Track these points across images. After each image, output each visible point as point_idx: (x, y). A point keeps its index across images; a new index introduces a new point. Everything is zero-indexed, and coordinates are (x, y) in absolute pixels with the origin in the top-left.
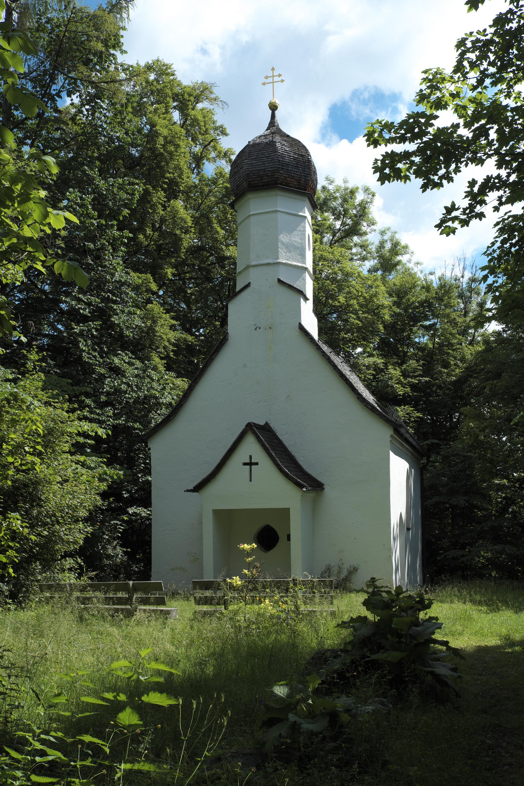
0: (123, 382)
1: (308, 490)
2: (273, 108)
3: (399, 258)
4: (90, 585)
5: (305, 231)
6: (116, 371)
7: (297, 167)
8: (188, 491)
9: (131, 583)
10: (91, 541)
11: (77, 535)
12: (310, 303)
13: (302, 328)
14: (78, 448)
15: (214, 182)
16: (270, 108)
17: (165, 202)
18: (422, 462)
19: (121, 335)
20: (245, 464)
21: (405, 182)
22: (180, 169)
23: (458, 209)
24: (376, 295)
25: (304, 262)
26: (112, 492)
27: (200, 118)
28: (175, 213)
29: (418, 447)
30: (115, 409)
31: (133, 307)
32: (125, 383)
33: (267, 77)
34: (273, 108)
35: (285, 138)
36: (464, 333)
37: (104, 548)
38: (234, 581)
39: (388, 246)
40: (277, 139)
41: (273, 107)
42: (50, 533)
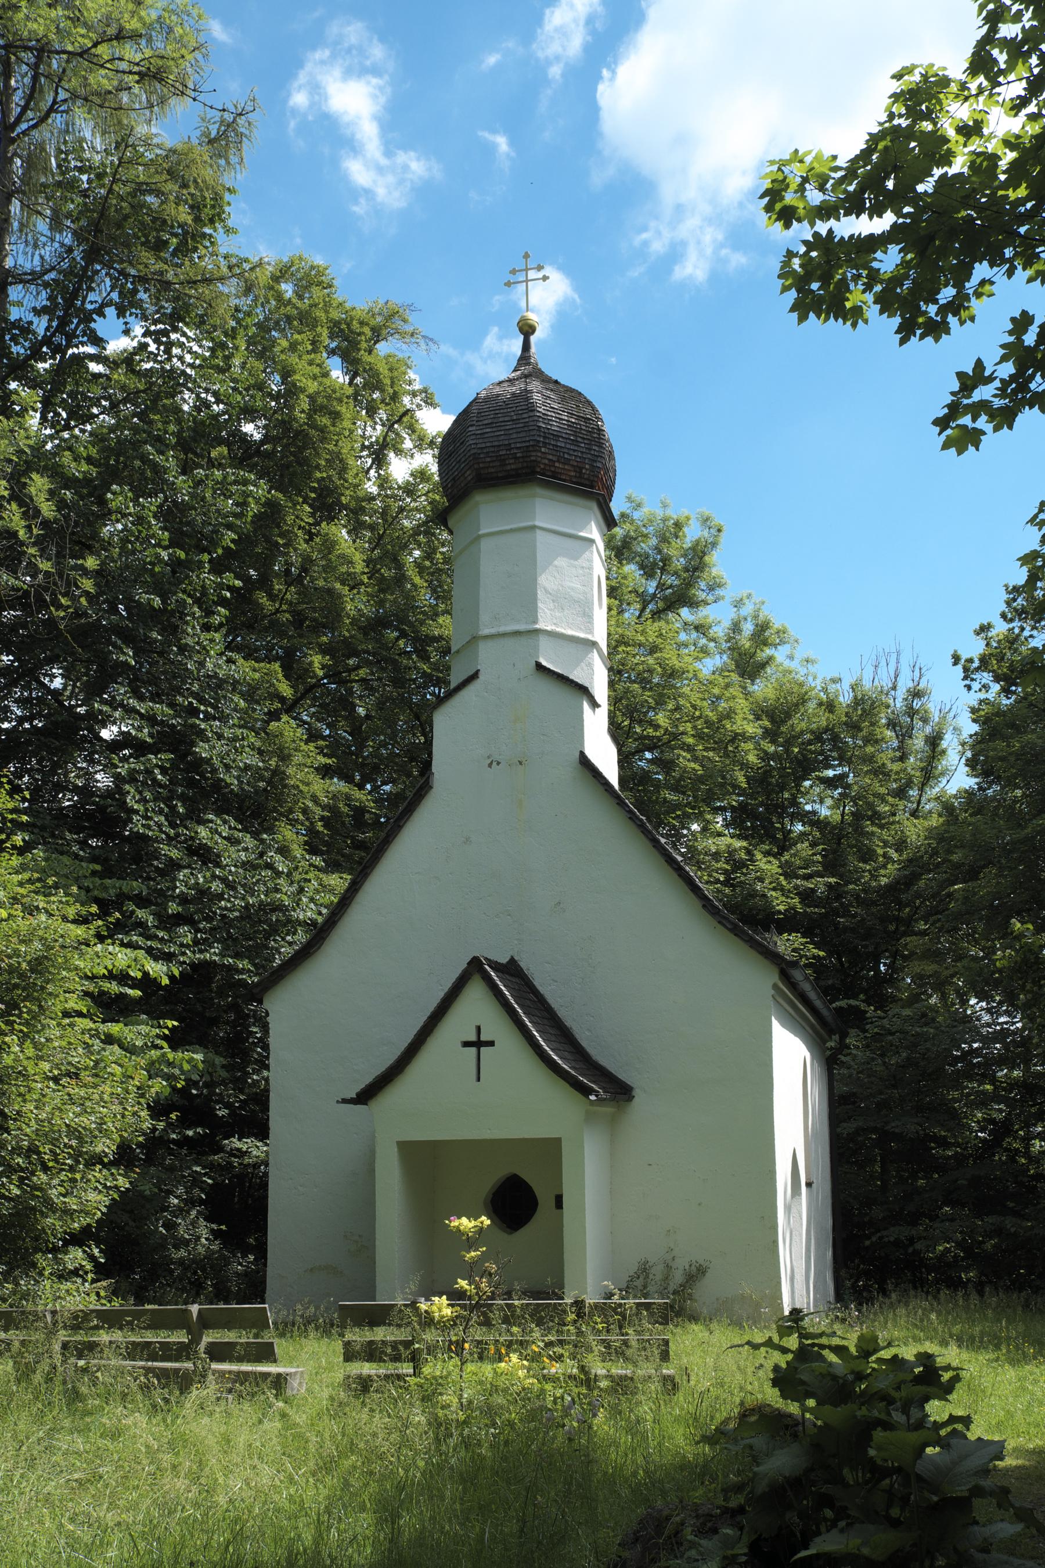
0: (214, 877)
1: (600, 1100)
3: (769, 651)
4: (100, 1314)
5: (591, 568)
6: (205, 855)
7: (575, 442)
8: (344, 1101)
9: (195, 1309)
10: (125, 1205)
11: (93, 1197)
12: (603, 712)
13: (585, 763)
14: (111, 1007)
15: (409, 490)
16: (521, 330)
17: (310, 524)
18: (829, 1044)
19: (218, 785)
20: (467, 1044)
21: (854, 325)
22: (341, 461)
23: (990, 379)
24: (729, 715)
25: (591, 632)
26: (183, 1105)
27: (383, 369)
28: (329, 545)
29: (825, 1012)
30: (198, 930)
31: (240, 727)
32: (219, 877)
33: (513, 272)
35: (551, 386)
36: (901, 793)
37: (170, 1226)
38: (434, 1308)
39: (748, 628)
40: (535, 385)
41: (526, 328)
42: (24, 1191)
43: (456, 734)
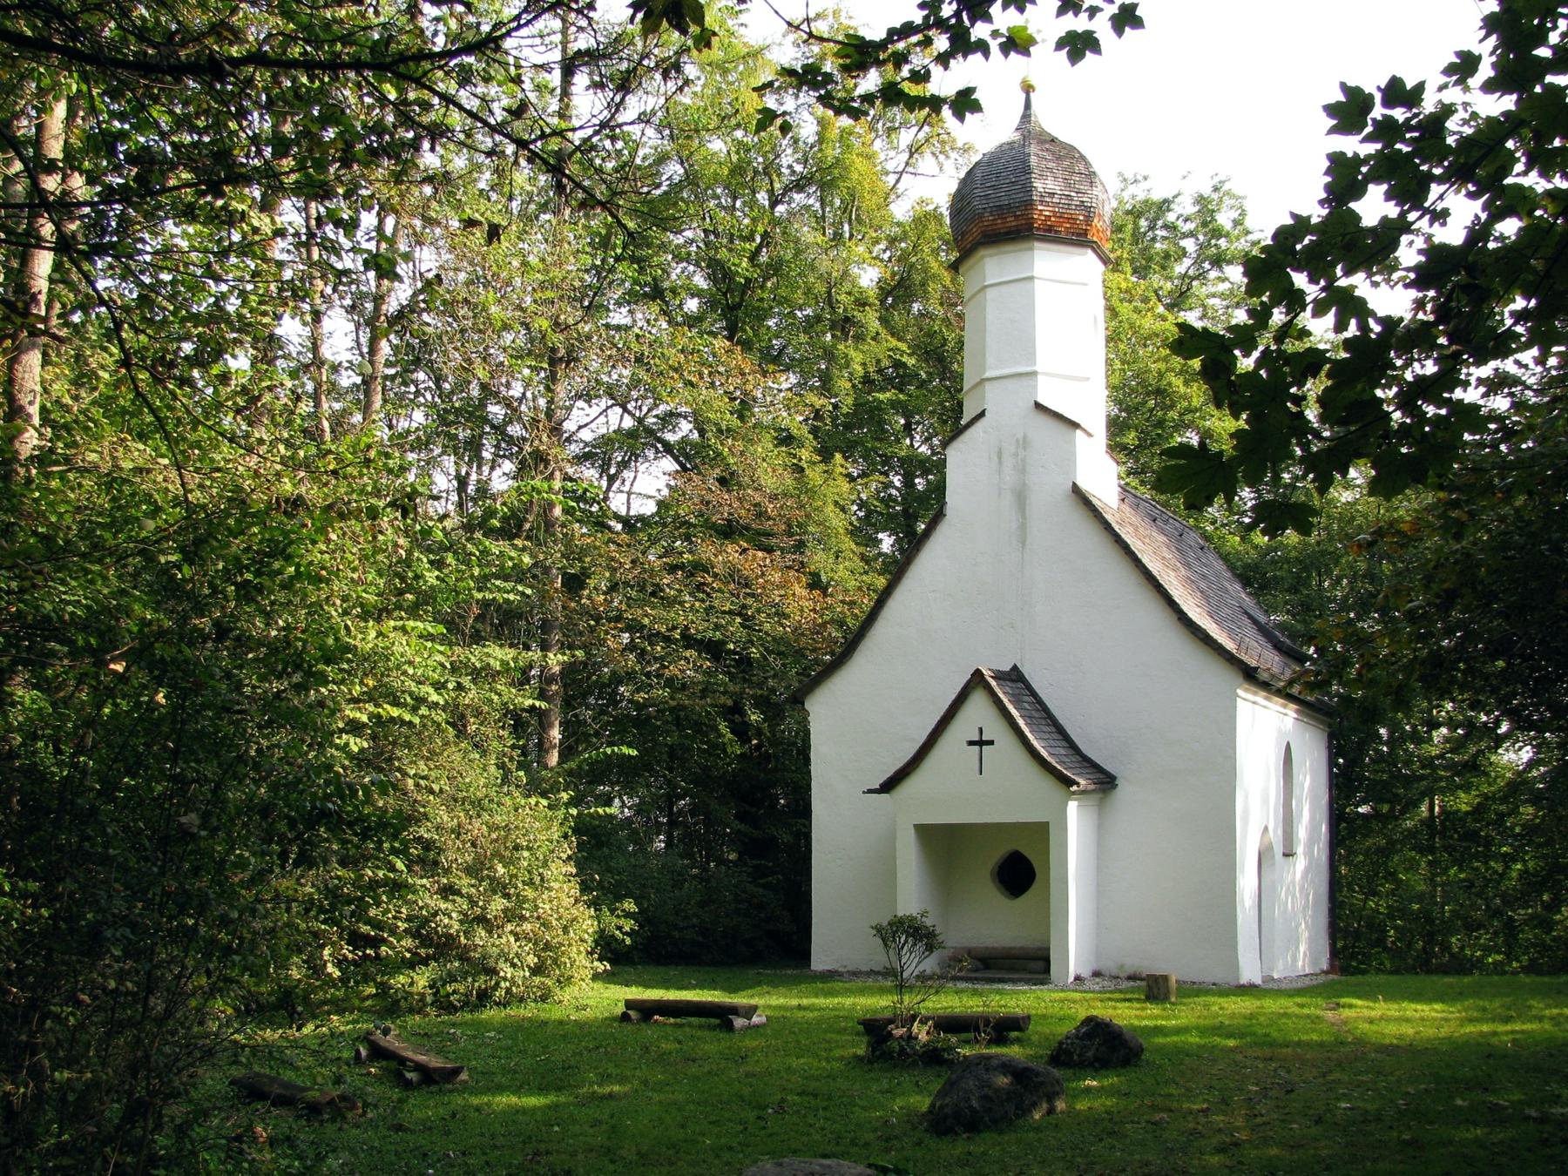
2: (1028, 89)
8: (870, 791)
13: (1081, 498)
20: (971, 743)
34: (1028, 89)
43: (968, 468)
